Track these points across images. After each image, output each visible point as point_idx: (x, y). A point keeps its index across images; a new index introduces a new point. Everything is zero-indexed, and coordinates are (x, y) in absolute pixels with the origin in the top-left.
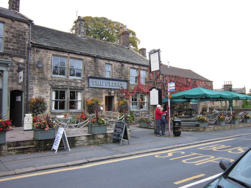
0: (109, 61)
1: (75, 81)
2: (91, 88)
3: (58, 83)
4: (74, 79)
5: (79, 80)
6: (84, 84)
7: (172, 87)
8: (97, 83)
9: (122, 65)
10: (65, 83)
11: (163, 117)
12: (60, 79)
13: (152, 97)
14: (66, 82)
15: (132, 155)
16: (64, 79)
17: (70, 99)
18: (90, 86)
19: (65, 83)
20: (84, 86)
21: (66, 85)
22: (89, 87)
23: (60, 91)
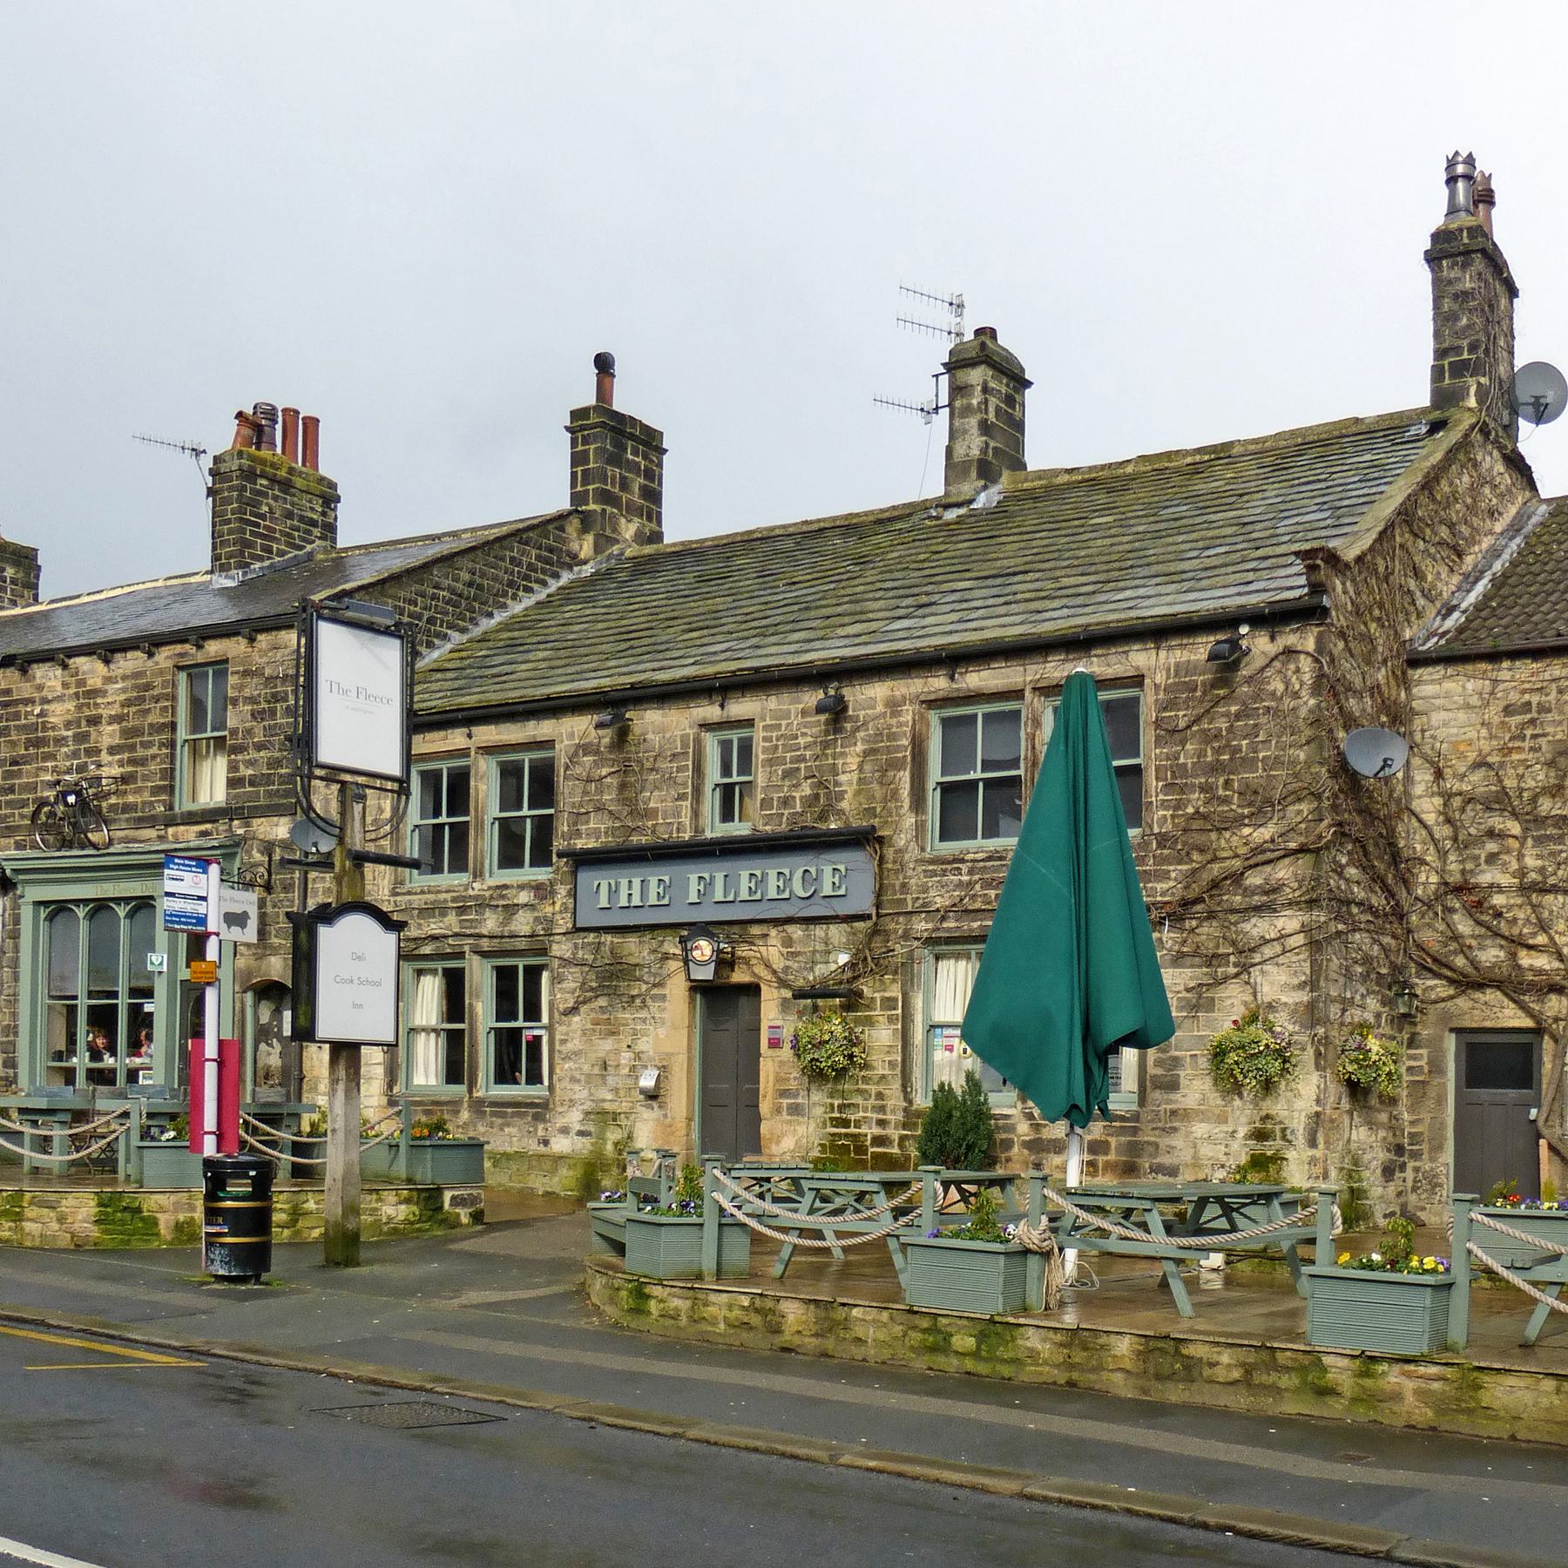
0: (952, 678)
1: (503, 897)
2: (591, 937)
3: (419, 926)
4: (498, 887)
5: (521, 887)
6: (549, 909)
7: (185, 896)
8: (624, 892)
9: (836, 712)
10: (452, 919)
11: (1205, 1275)
12: (431, 897)
13: (378, 984)
14: (462, 910)
15: (50, 1326)
16: (448, 896)
17: (117, 1005)
18: (578, 925)
19: (452, 919)
20: (550, 922)
21: (457, 930)
22: (577, 930)
23: (526, 968)
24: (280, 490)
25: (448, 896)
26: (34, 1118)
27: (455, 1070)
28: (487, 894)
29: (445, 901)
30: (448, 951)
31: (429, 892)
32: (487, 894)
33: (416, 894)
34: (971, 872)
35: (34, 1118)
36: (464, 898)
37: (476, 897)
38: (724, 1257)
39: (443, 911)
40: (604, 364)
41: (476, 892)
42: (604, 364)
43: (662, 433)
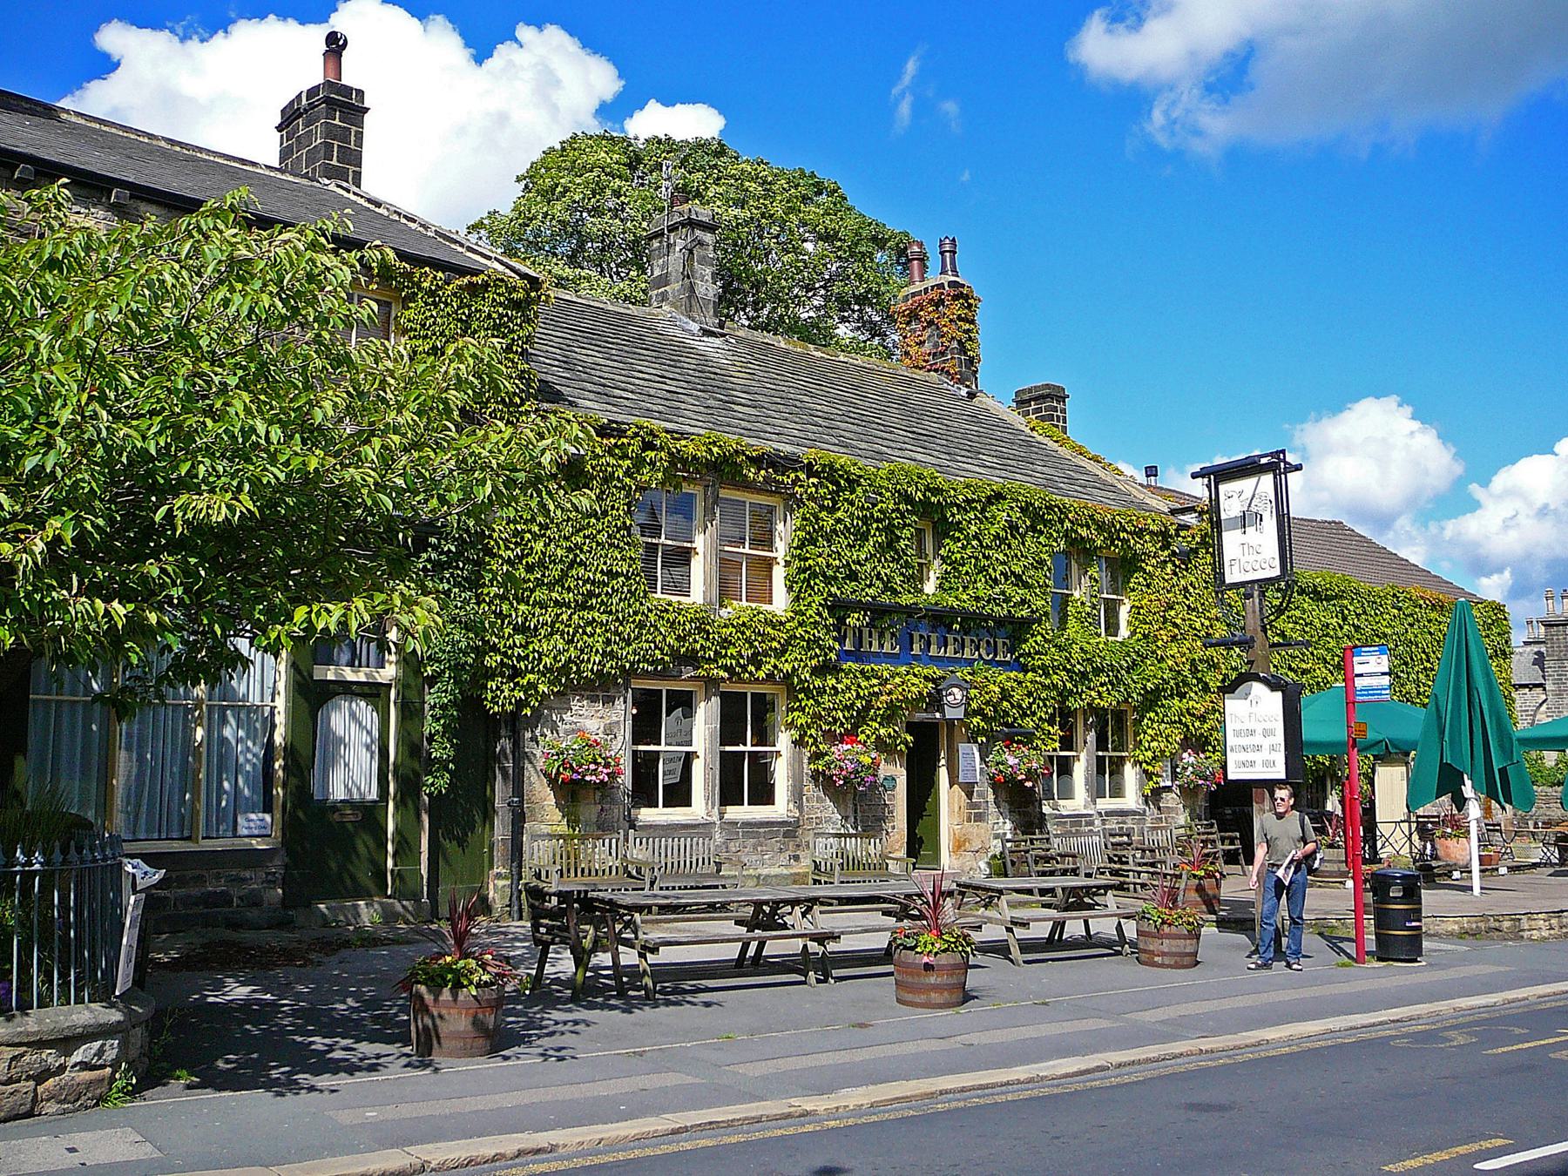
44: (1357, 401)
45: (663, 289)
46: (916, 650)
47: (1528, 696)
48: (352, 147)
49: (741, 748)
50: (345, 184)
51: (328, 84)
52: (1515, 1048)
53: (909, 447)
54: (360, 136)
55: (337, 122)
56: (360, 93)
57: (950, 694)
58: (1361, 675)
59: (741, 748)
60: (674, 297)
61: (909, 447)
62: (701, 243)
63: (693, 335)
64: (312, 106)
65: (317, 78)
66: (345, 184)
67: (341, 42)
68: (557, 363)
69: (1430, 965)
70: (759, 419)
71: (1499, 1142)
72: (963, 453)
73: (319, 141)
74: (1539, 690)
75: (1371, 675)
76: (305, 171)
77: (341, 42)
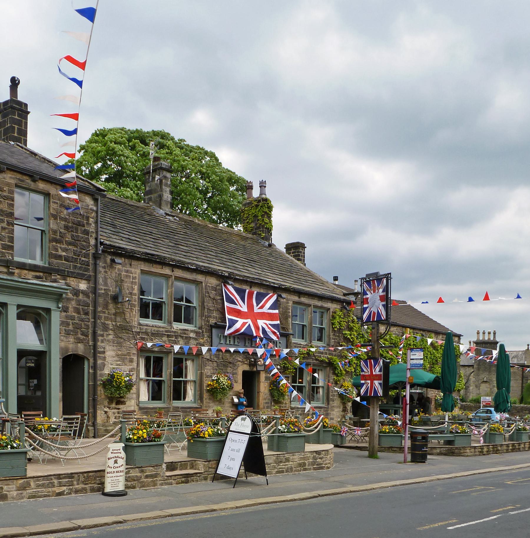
1: (185, 334)
5: (192, 331)
14: (168, 336)
16: (163, 329)
24: (293, 250)
25: (163, 329)
26: (13, 450)
27: (156, 395)
28: (179, 331)
29: (163, 331)
30: (165, 351)
31: (155, 327)
32: (179, 331)
33: (150, 326)
34: (357, 364)
35: (13, 450)
36: (170, 332)
37: (175, 332)
38: (137, 448)
39: (162, 335)
40: (14, 83)
41: (175, 330)
42: (14, 83)
43: (286, 245)
44: (63, 165)
45: (149, 196)
46: (228, 342)
47: (467, 370)
48: (23, 129)
49: (181, 379)
50: (20, 144)
51: (11, 100)
52: (466, 490)
53: (246, 265)
54: (26, 124)
55: (16, 117)
56: (26, 105)
57: (259, 361)
58: (413, 359)
59: (181, 379)
60: (154, 199)
61: (246, 265)
62: (165, 177)
63: (162, 216)
64: (5, 109)
65: (8, 98)
66: (20, 144)
67: (17, 82)
68: (109, 225)
69: (429, 464)
70: (189, 252)
71: (454, 521)
72: (266, 268)
73: (9, 125)
74: (471, 368)
75: (416, 359)
76: (3, 138)
77: (17, 82)
